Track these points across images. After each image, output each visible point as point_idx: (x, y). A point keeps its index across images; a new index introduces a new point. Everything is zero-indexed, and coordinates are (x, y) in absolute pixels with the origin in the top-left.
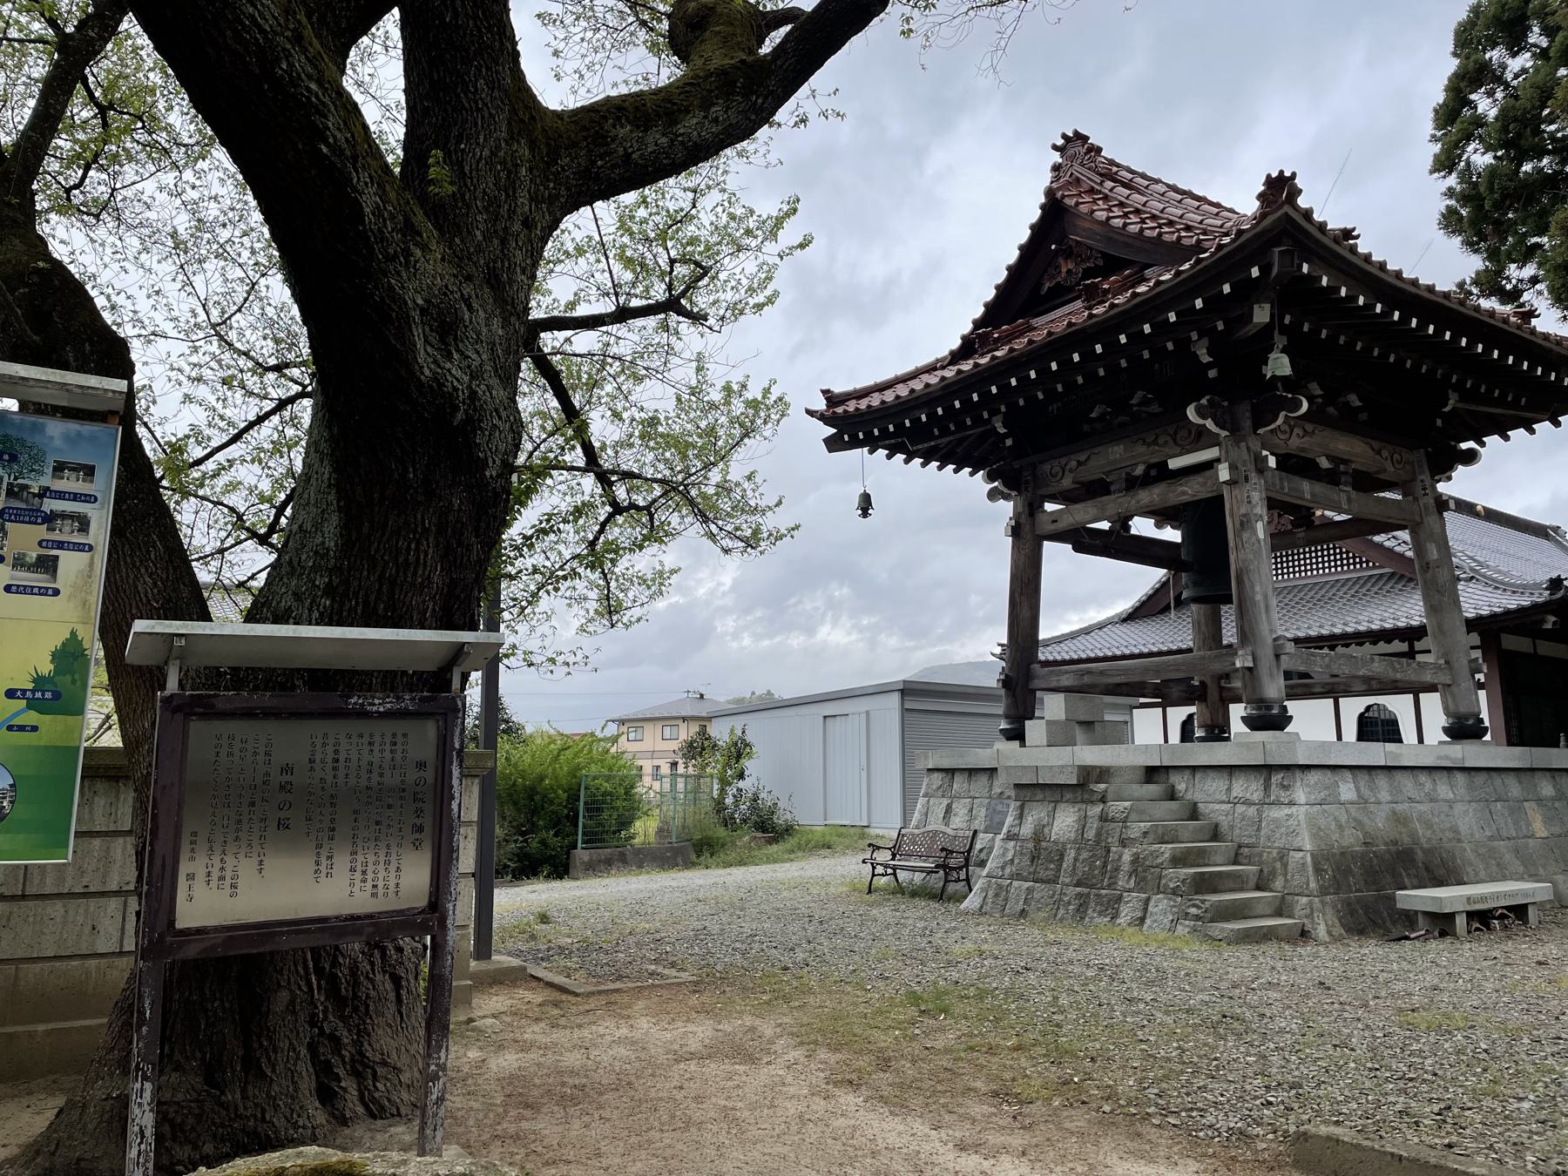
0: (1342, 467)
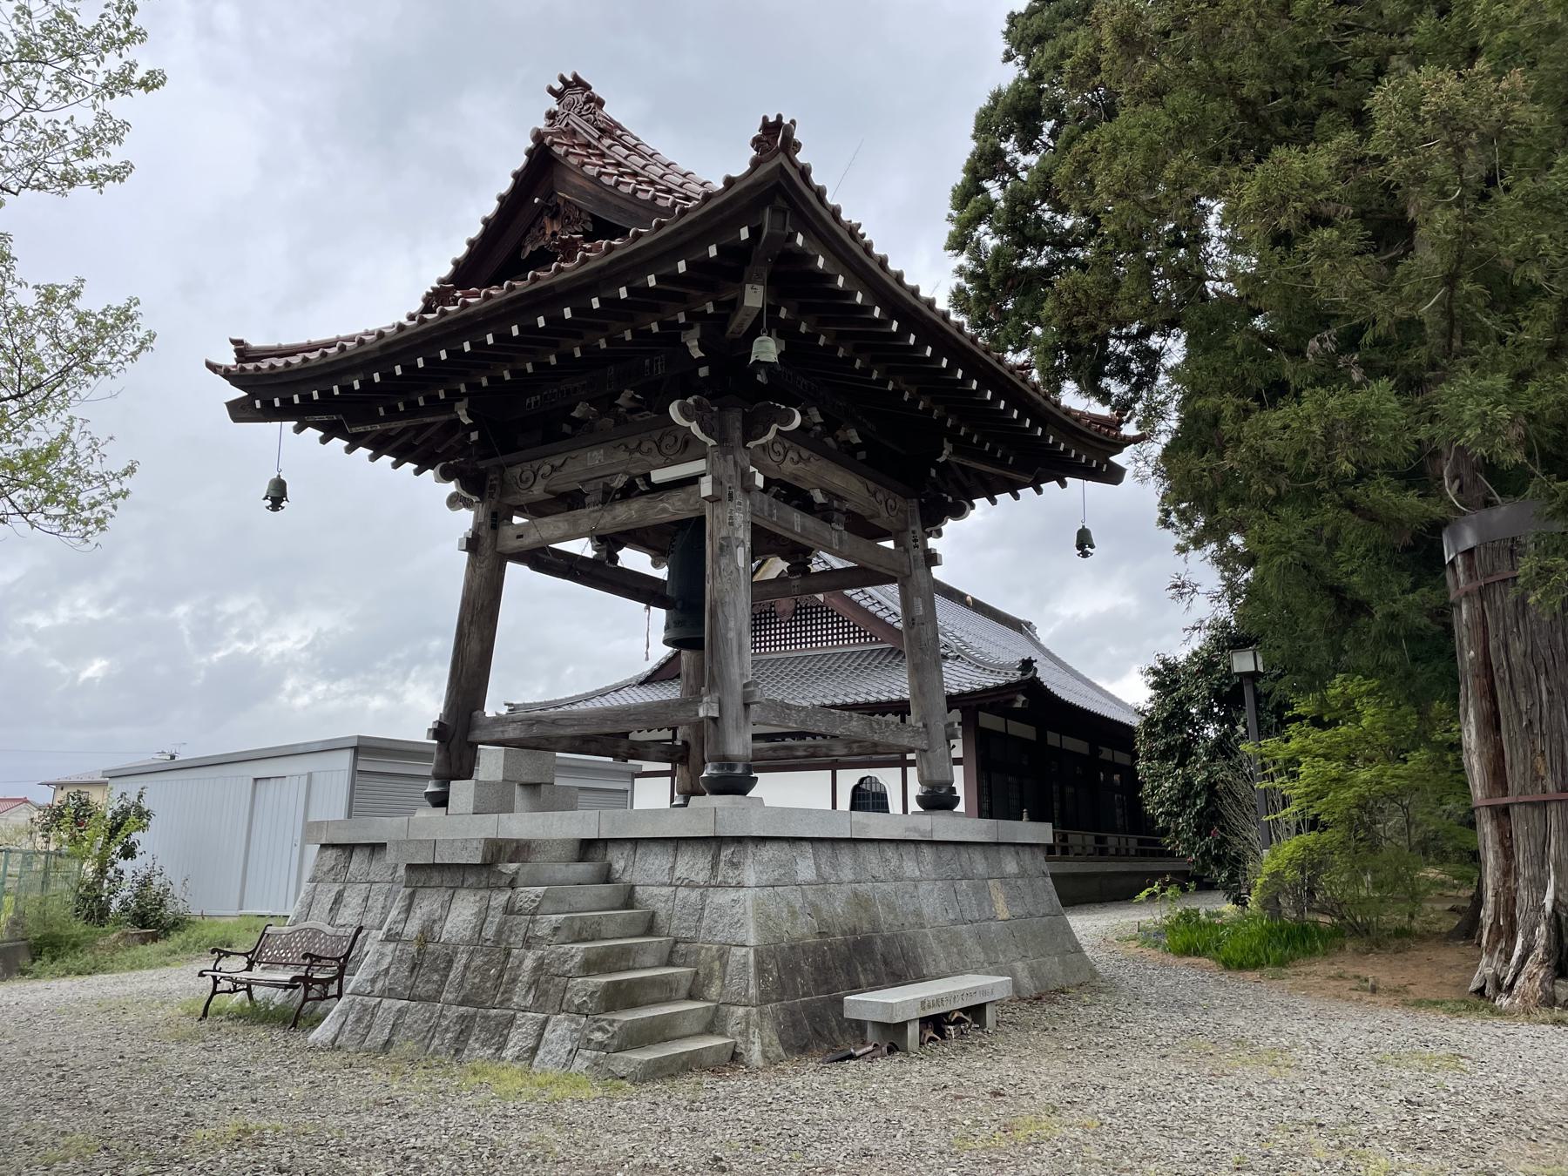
0: (836, 503)
